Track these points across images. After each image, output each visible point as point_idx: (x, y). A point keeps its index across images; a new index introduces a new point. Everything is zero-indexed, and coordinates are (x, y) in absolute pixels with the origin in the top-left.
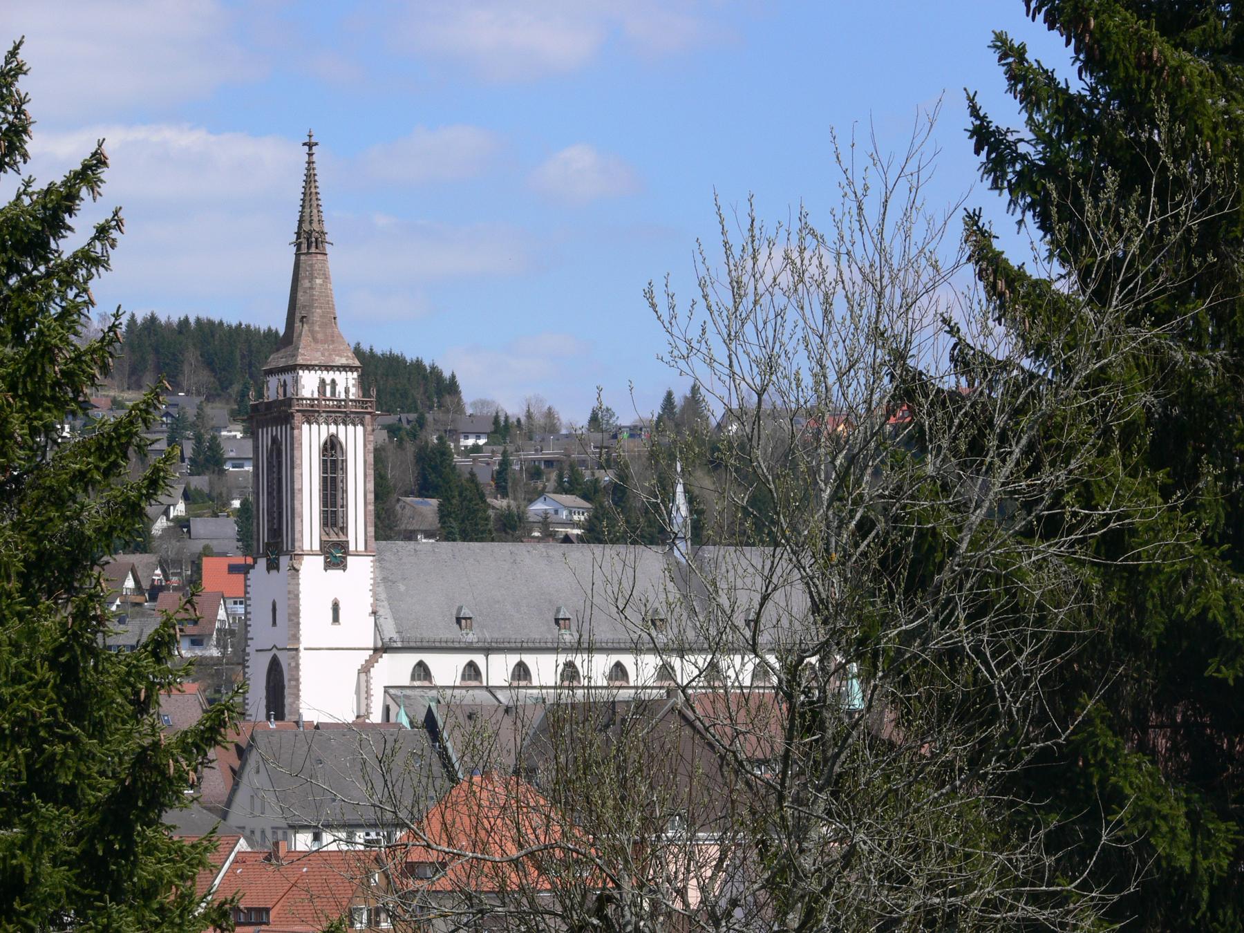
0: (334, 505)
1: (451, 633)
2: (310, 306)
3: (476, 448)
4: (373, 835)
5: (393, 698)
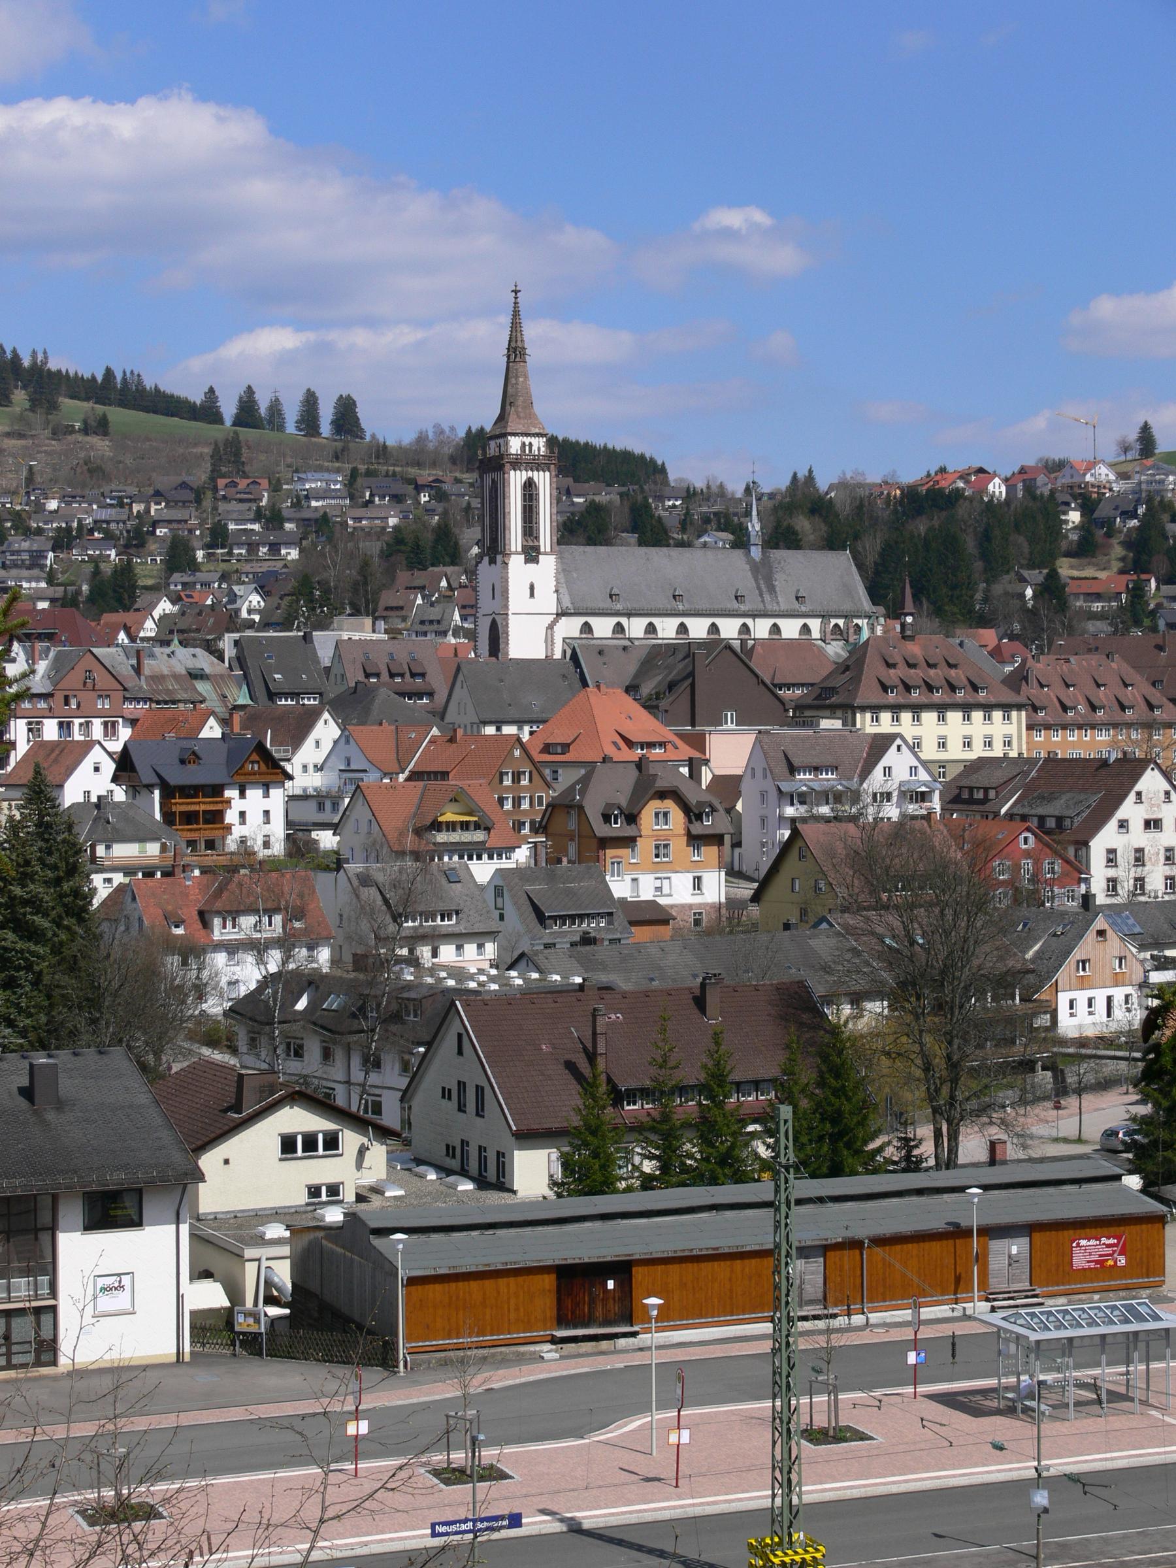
0: (531, 522)
1: (607, 604)
2: (516, 395)
3: (674, 506)
4: (535, 728)
5: (568, 645)
